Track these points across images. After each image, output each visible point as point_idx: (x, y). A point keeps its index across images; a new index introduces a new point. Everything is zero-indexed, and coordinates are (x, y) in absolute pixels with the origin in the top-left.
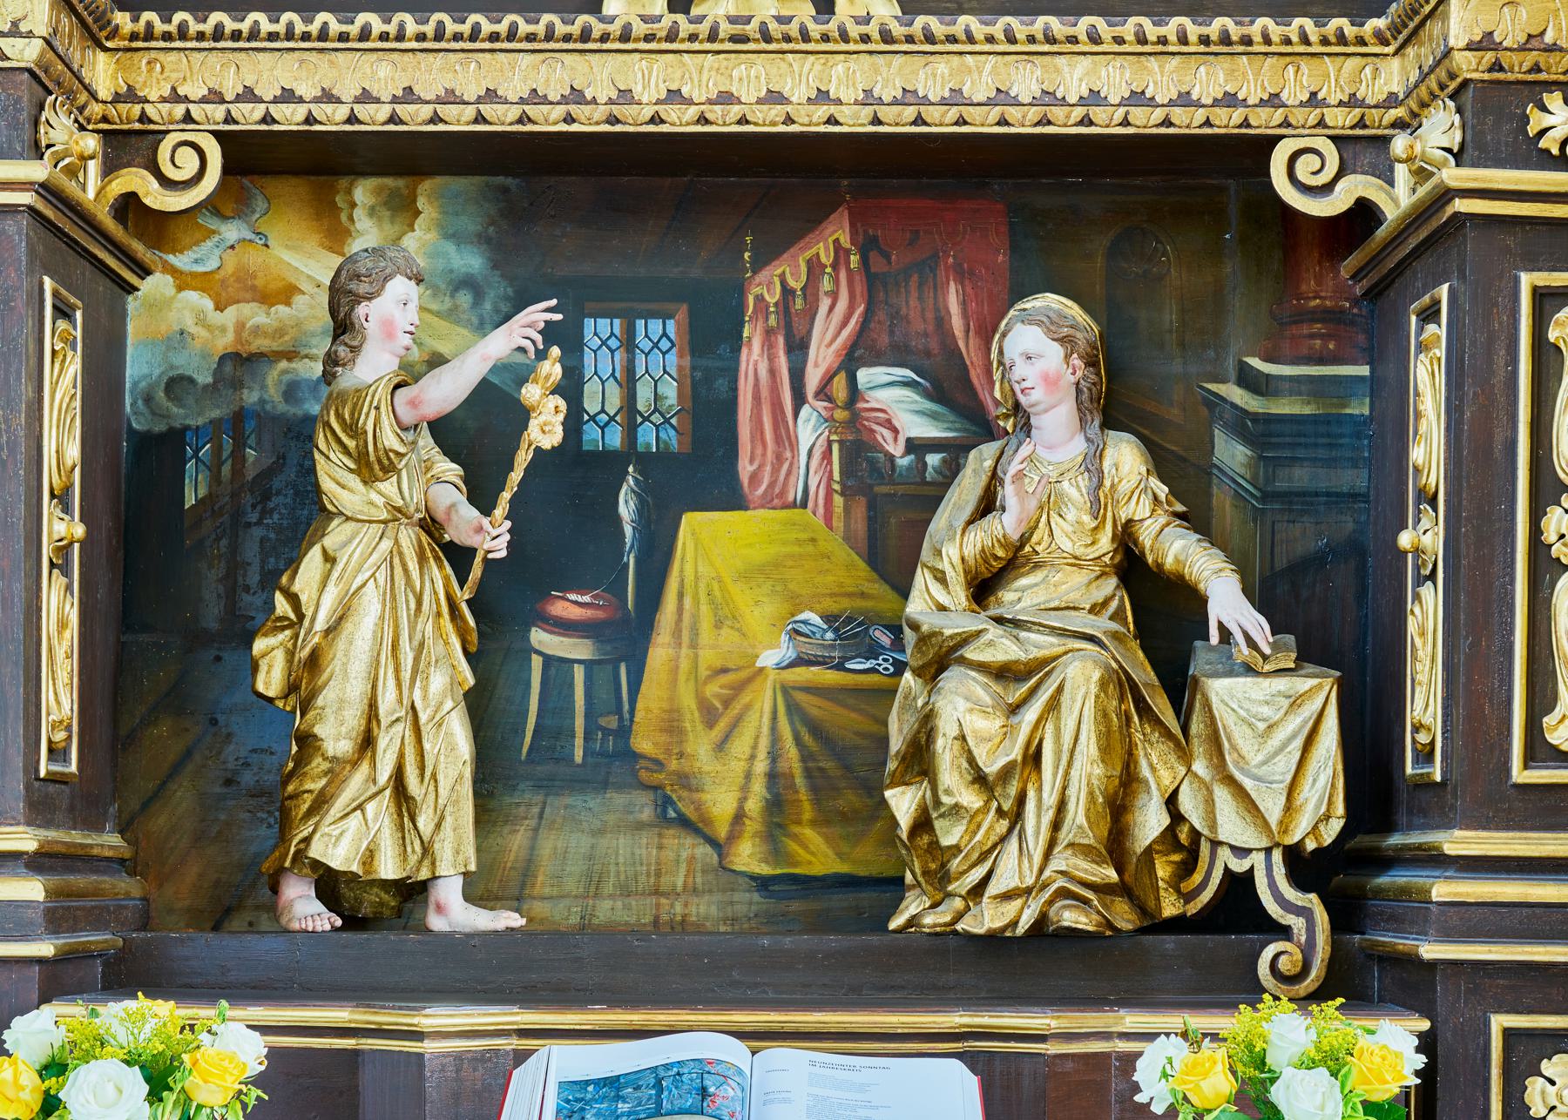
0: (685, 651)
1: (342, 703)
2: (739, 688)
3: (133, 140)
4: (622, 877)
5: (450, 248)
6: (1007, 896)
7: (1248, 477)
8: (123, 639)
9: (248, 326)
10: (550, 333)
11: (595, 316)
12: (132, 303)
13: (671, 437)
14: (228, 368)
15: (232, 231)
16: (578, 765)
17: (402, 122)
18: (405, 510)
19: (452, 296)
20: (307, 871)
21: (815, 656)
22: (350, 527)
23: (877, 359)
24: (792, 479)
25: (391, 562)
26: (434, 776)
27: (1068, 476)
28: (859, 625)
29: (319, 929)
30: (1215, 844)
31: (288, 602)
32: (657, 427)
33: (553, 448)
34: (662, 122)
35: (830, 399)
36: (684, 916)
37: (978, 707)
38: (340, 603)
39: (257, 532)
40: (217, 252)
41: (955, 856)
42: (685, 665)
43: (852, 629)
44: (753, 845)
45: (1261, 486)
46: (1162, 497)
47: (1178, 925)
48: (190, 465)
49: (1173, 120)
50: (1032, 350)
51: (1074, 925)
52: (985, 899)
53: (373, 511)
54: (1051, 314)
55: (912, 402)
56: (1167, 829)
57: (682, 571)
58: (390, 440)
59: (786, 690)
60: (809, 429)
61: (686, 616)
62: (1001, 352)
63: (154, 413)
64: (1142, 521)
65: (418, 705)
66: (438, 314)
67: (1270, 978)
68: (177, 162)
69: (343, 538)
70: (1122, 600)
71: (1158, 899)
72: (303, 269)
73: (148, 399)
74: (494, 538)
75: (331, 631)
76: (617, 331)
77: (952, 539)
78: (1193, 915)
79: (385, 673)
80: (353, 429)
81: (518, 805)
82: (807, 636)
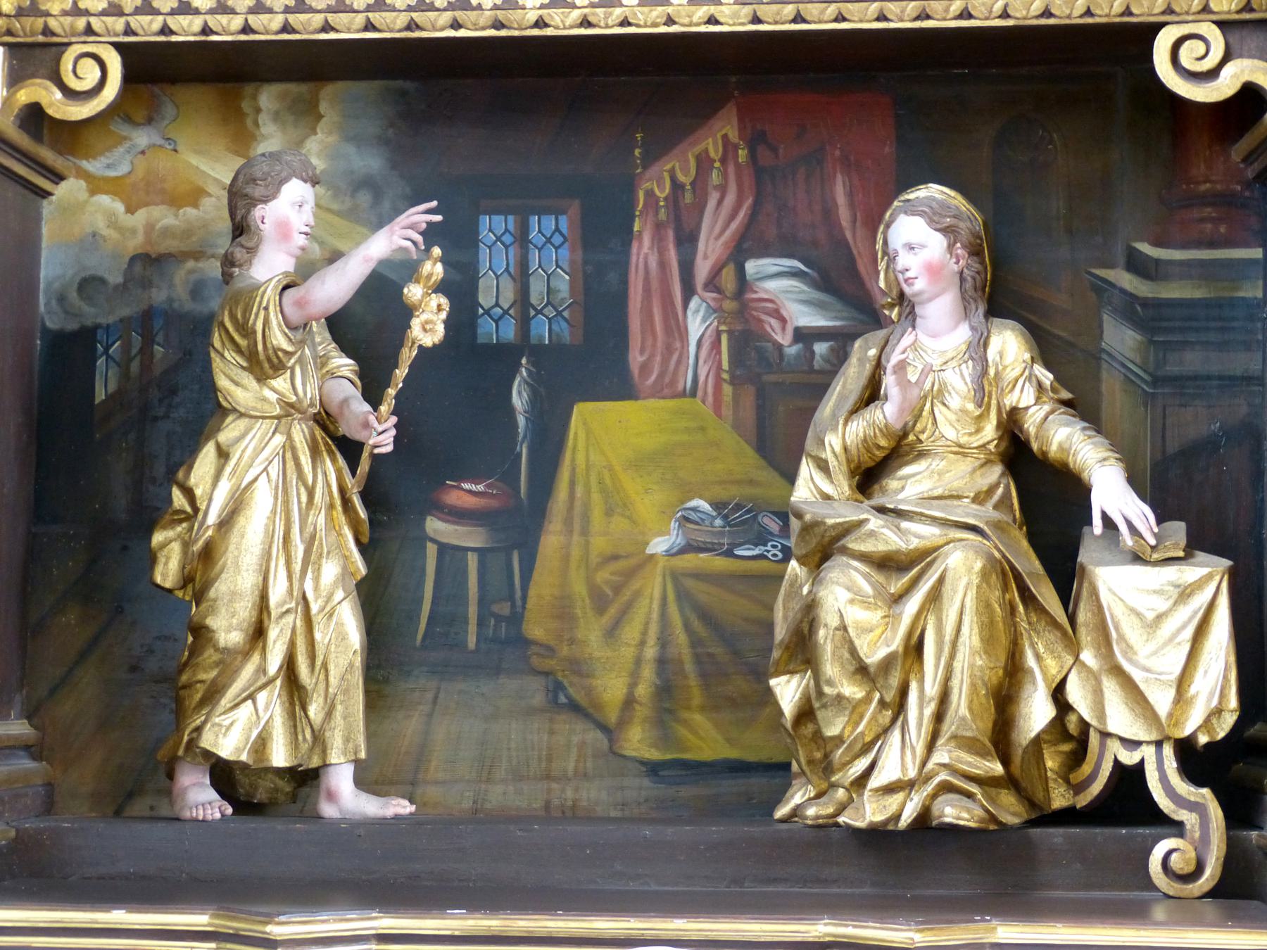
0: (576, 538)
1: (234, 595)
2: (630, 574)
3: (37, 51)
4: (514, 762)
5: (351, 149)
6: (890, 789)
7: (1138, 361)
8: (33, 530)
9: (157, 227)
10: (431, 234)
11: (490, 213)
12: (47, 207)
13: (563, 329)
14: (138, 268)
15: (142, 138)
16: (472, 652)
17: (294, 31)
18: (298, 406)
19: (353, 196)
20: (200, 759)
21: (705, 543)
22: (242, 424)
23: (764, 251)
24: (682, 368)
25: (284, 457)
26: (325, 666)
27: (954, 363)
28: (748, 512)
29: (209, 818)
30: (1105, 735)
31: (185, 496)
32: (550, 320)
33: (434, 345)
34: (547, 25)
35: (718, 290)
36: (575, 801)
37: (858, 599)
38: (232, 498)
39: (165, 426)
40: (128, 157)
41: (838, 747)
42: (576, 553)
43: (741, 516)
44: (643, 731)
45: (1151, 370)
46: (1047, 383)
47: (1068, 817)
48: (101, 362)
49: (1053, 11)
50: (914, 240)
51: (955, 822)
52: (867, 794)
53: (266, 407)
54: (934, 204)
55: (800, 292)
56: (1054, 719)
57: (573, 460)
58: (279, 339)
59: (676, 577)
60: (697, 323)
61: (578, 504)
62: (885, 242)
63: (66, 312)
64: (1027, 408)
65: (310, 596)
66: (338, 213)
67: (1162, 876)
68: (79, 71)
69: (236, 433)
70: (1007, 488)
71: (1047, 790)
72: (212, 173)
73: (62, 299)
74: (380, 434)
75: (226, 523)
76: (511, 227)
77: (835, 429)
78: (1081, 808)
79: (276, 566)
80: (247, 332)
81: (413, 690)
82: (696, 523)
